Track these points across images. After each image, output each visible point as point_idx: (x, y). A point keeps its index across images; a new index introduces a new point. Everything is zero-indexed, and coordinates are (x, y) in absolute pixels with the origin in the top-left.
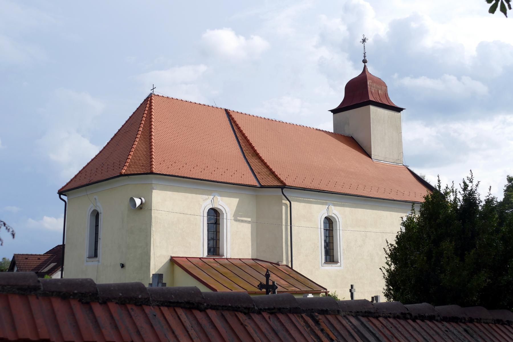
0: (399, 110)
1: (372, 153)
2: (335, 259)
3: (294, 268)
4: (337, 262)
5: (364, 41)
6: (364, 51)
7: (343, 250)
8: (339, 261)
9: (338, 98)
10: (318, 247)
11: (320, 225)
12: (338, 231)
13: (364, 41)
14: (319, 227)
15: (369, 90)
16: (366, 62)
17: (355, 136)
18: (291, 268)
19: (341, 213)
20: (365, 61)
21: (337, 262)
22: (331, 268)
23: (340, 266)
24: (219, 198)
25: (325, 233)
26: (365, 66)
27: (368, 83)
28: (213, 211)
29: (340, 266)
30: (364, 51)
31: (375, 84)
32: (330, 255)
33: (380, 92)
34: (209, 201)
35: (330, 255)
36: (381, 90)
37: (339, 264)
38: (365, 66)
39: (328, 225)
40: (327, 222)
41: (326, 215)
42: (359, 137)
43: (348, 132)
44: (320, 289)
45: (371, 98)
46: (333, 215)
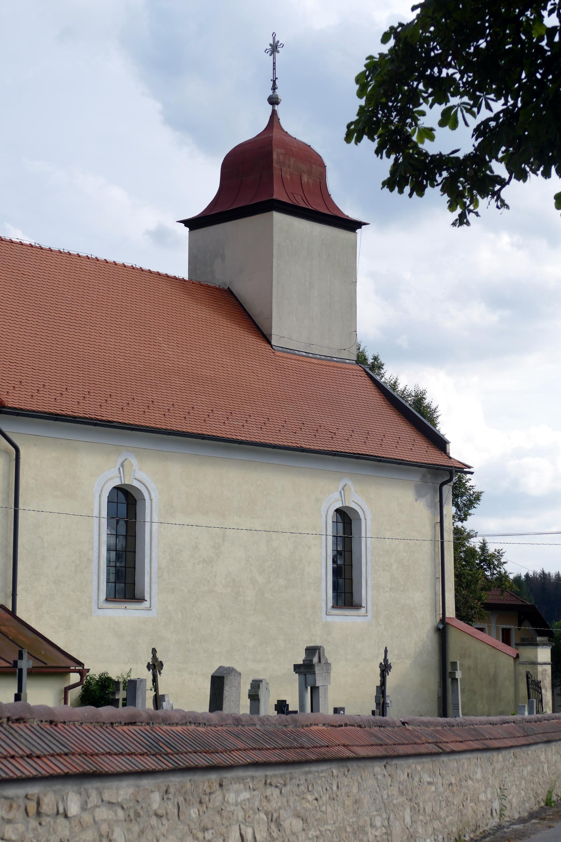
0: (353, 226)
1: (274, 331)
2: (137, 592)
3: (19, 614)
4: (142, 600)
5: (274, 48)
6: (274, 74)
7: (159, 568)
8: (147, 597)
9: (203, 187)
10: (89, 561)
11: (99, 506)
12: (363, 540)
13: (274, 48)
14: (96, 513)
15: (276, 173)
16: (278, 103)
17: (238, 289)
18: (13, 613)
19: (157, 475)
20: (273, 101)
21: (142, 600)
22: (125, 614)
23: (149, 609)
24: (133, 461)
25: (335, 543)
26: (274, 113)
27: (275, 156)
28: (121, 495)
29: (149, 609)
30: (274, 74)
31: (292, 160)
32: (124, 582)
33: (305, 178)
34: (115, 472)
35: (124, 582)
36: (310, 173)
37: (146, 604)
38: (274, 113)
39: (341, 525)
40: (340, 520)
41: (117, 483)
42: (245, 289)
43: (220, 277)
44: (69, 663)
45: (279, 194)
46: (136, 484)
